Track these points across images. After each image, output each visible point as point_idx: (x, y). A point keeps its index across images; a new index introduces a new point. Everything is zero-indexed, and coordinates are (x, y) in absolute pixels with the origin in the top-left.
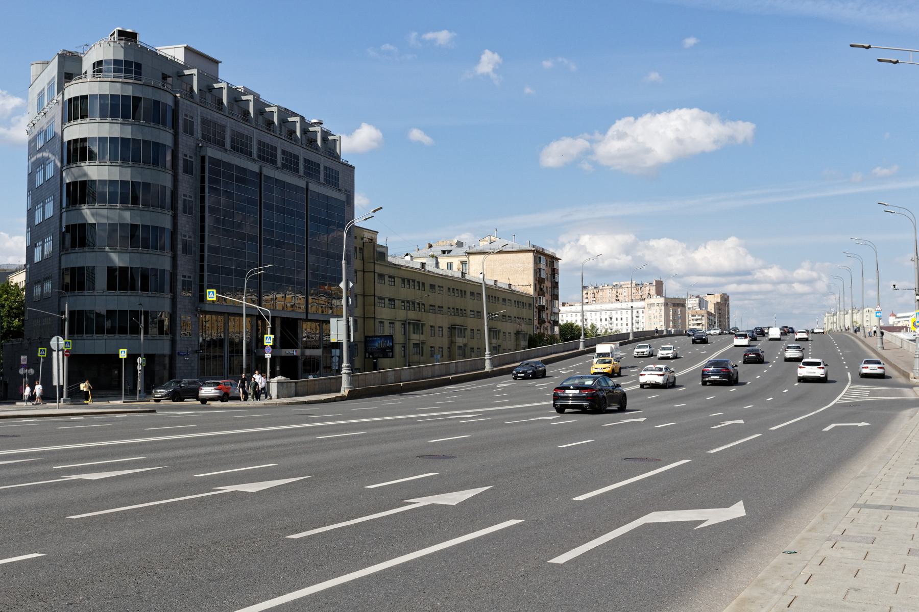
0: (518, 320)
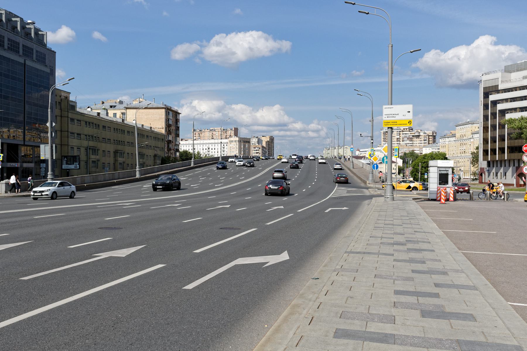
0: (156, 148)
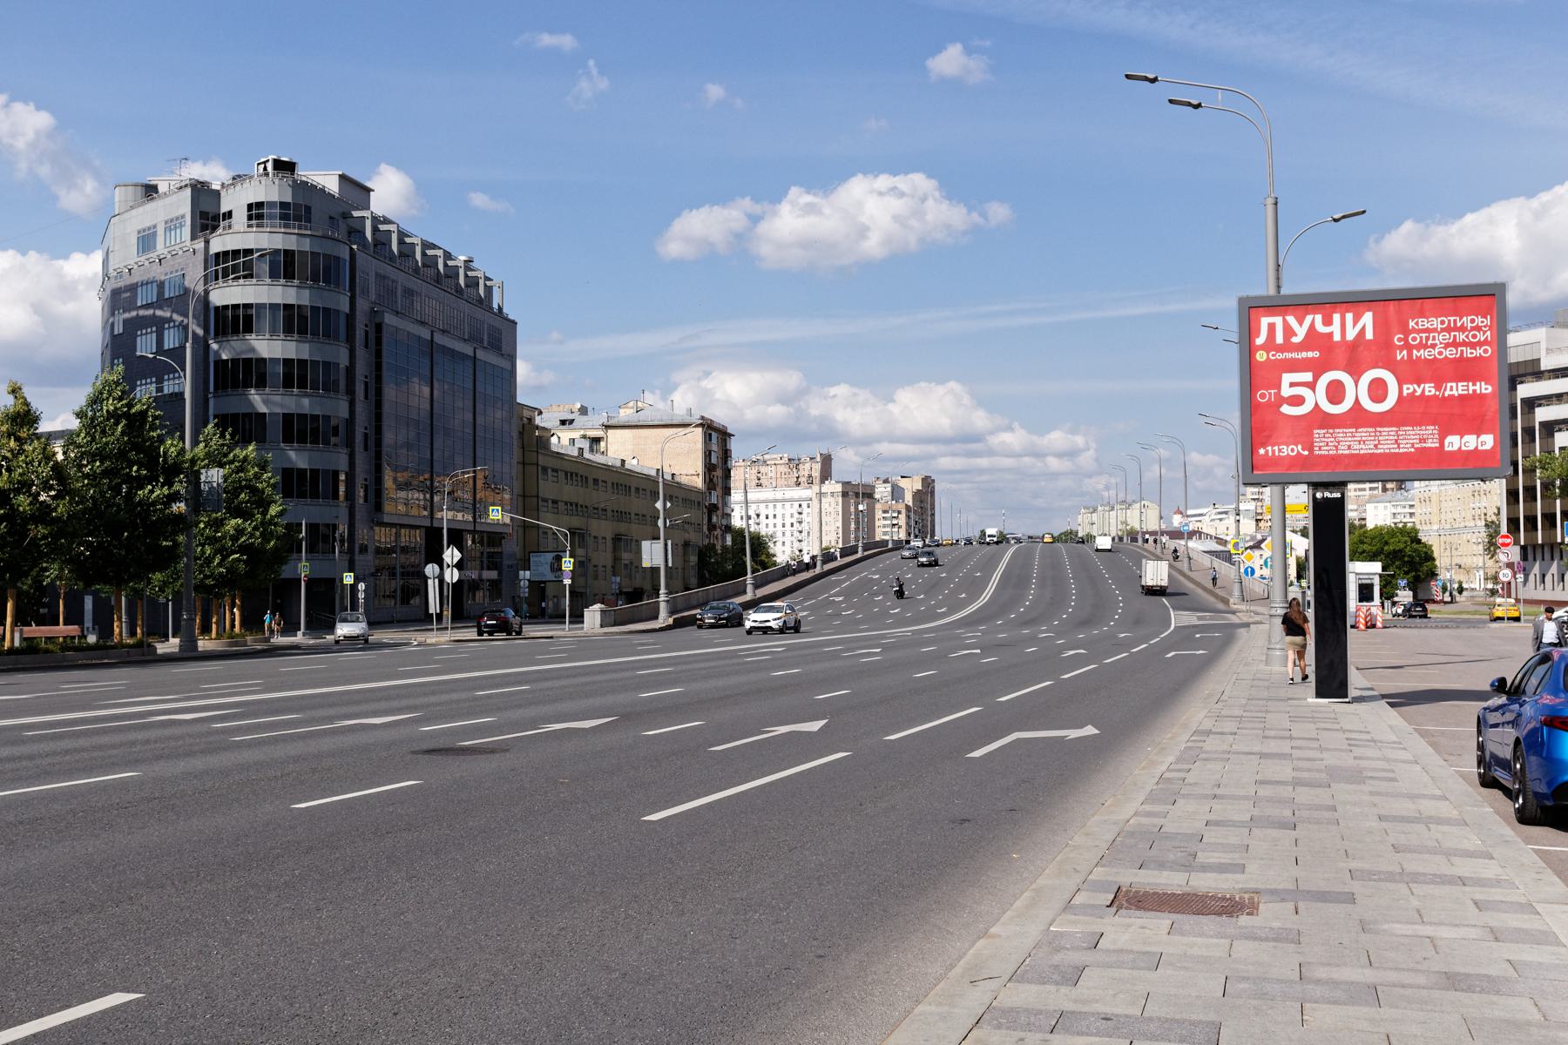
0: (686, 526)
